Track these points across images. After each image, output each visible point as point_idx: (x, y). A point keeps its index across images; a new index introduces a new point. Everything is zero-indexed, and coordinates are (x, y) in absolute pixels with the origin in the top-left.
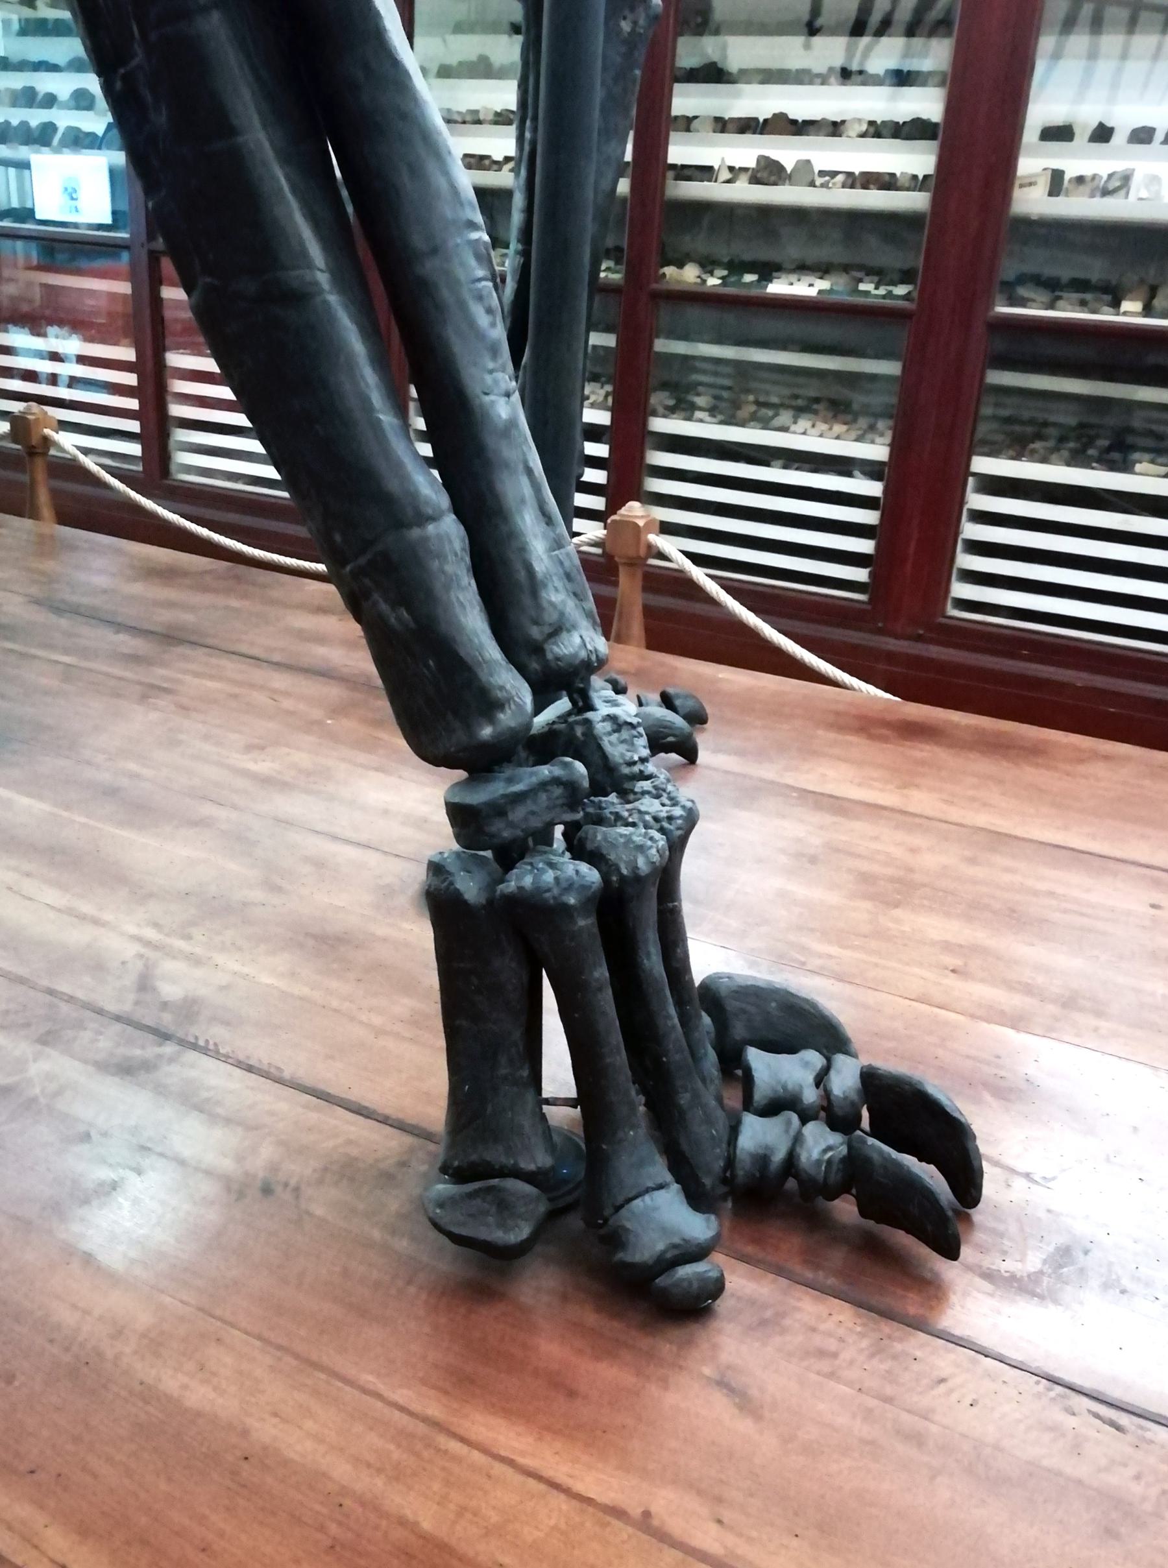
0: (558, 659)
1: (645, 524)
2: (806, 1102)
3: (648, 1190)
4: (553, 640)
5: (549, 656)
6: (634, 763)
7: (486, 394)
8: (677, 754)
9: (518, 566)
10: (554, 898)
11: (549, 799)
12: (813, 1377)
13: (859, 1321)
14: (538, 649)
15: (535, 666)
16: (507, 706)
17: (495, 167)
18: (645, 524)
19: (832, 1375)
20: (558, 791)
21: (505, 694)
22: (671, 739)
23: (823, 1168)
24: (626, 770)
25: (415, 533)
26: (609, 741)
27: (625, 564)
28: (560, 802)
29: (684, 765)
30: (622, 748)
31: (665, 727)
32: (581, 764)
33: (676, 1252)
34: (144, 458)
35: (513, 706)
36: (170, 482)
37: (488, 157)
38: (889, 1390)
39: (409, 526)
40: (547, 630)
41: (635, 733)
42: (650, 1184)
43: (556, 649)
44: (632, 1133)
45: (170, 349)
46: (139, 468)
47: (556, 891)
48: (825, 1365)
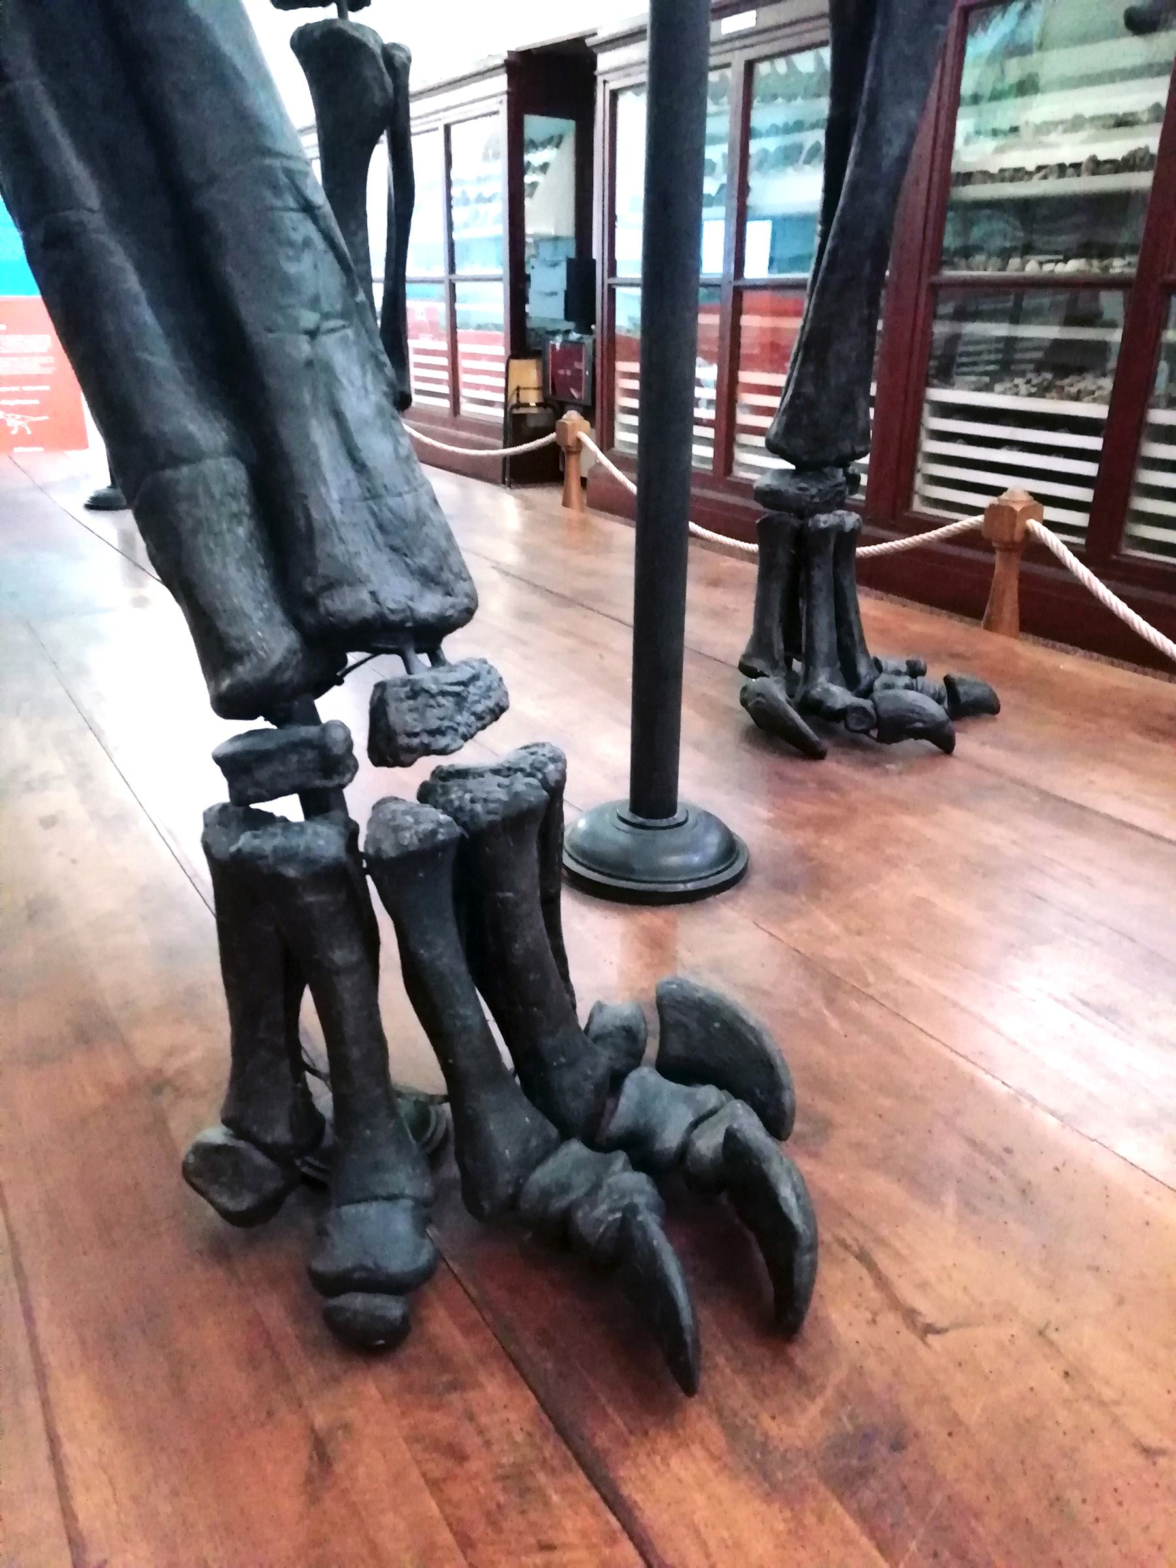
0: (329, 614)
1: (1021, 510)
2: (658, 1146)
3: (376, 1198)
4: (327, 593)
5: (322, 610)
6: (416, 735)
7: (271, 331)
8: (933, 742)
9: (299, 514)
10: (268, 866)
11: (299, 762)
12: (415, 1476)
13: (528, 1427)
14: (311, 602)
15: (309, 619)
16: (246, 658)
17: (1026, 177)
18: (1022, 510)
19: (435, 1485)
20: (310, 755)
21: (243, 645)
22: (919, 725)
23: (601, 1230)
24: (403, 740)
25: (169, 473)
26: (396, 708)
27: (1000, 549)
28: (311, 766)
29: (934, 755)
30: (409, 718)
31: (913, 712)
32: (928, 742)
33: (363, 1274)
34: (715, 460)
35: (255, 659)
36: (732, 479)
37: (1023, 168)
38: (479, 1530)
39: (163, 467)
40: (320, 582)
41: (432, 702)
42: (381, 1191)
43: (328, 602)
44: (368, 1132)
45: (618, 360)
46: (709, 467)
47: (271, 861)
48: (438, 1467)
